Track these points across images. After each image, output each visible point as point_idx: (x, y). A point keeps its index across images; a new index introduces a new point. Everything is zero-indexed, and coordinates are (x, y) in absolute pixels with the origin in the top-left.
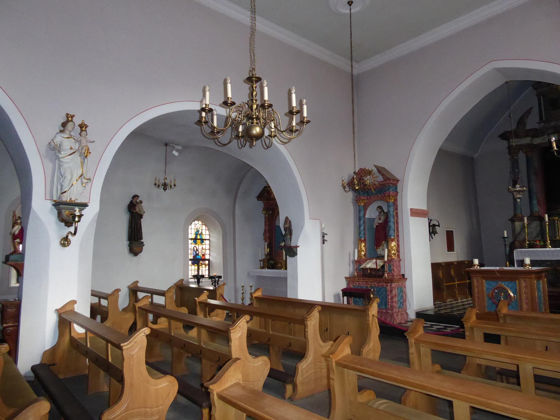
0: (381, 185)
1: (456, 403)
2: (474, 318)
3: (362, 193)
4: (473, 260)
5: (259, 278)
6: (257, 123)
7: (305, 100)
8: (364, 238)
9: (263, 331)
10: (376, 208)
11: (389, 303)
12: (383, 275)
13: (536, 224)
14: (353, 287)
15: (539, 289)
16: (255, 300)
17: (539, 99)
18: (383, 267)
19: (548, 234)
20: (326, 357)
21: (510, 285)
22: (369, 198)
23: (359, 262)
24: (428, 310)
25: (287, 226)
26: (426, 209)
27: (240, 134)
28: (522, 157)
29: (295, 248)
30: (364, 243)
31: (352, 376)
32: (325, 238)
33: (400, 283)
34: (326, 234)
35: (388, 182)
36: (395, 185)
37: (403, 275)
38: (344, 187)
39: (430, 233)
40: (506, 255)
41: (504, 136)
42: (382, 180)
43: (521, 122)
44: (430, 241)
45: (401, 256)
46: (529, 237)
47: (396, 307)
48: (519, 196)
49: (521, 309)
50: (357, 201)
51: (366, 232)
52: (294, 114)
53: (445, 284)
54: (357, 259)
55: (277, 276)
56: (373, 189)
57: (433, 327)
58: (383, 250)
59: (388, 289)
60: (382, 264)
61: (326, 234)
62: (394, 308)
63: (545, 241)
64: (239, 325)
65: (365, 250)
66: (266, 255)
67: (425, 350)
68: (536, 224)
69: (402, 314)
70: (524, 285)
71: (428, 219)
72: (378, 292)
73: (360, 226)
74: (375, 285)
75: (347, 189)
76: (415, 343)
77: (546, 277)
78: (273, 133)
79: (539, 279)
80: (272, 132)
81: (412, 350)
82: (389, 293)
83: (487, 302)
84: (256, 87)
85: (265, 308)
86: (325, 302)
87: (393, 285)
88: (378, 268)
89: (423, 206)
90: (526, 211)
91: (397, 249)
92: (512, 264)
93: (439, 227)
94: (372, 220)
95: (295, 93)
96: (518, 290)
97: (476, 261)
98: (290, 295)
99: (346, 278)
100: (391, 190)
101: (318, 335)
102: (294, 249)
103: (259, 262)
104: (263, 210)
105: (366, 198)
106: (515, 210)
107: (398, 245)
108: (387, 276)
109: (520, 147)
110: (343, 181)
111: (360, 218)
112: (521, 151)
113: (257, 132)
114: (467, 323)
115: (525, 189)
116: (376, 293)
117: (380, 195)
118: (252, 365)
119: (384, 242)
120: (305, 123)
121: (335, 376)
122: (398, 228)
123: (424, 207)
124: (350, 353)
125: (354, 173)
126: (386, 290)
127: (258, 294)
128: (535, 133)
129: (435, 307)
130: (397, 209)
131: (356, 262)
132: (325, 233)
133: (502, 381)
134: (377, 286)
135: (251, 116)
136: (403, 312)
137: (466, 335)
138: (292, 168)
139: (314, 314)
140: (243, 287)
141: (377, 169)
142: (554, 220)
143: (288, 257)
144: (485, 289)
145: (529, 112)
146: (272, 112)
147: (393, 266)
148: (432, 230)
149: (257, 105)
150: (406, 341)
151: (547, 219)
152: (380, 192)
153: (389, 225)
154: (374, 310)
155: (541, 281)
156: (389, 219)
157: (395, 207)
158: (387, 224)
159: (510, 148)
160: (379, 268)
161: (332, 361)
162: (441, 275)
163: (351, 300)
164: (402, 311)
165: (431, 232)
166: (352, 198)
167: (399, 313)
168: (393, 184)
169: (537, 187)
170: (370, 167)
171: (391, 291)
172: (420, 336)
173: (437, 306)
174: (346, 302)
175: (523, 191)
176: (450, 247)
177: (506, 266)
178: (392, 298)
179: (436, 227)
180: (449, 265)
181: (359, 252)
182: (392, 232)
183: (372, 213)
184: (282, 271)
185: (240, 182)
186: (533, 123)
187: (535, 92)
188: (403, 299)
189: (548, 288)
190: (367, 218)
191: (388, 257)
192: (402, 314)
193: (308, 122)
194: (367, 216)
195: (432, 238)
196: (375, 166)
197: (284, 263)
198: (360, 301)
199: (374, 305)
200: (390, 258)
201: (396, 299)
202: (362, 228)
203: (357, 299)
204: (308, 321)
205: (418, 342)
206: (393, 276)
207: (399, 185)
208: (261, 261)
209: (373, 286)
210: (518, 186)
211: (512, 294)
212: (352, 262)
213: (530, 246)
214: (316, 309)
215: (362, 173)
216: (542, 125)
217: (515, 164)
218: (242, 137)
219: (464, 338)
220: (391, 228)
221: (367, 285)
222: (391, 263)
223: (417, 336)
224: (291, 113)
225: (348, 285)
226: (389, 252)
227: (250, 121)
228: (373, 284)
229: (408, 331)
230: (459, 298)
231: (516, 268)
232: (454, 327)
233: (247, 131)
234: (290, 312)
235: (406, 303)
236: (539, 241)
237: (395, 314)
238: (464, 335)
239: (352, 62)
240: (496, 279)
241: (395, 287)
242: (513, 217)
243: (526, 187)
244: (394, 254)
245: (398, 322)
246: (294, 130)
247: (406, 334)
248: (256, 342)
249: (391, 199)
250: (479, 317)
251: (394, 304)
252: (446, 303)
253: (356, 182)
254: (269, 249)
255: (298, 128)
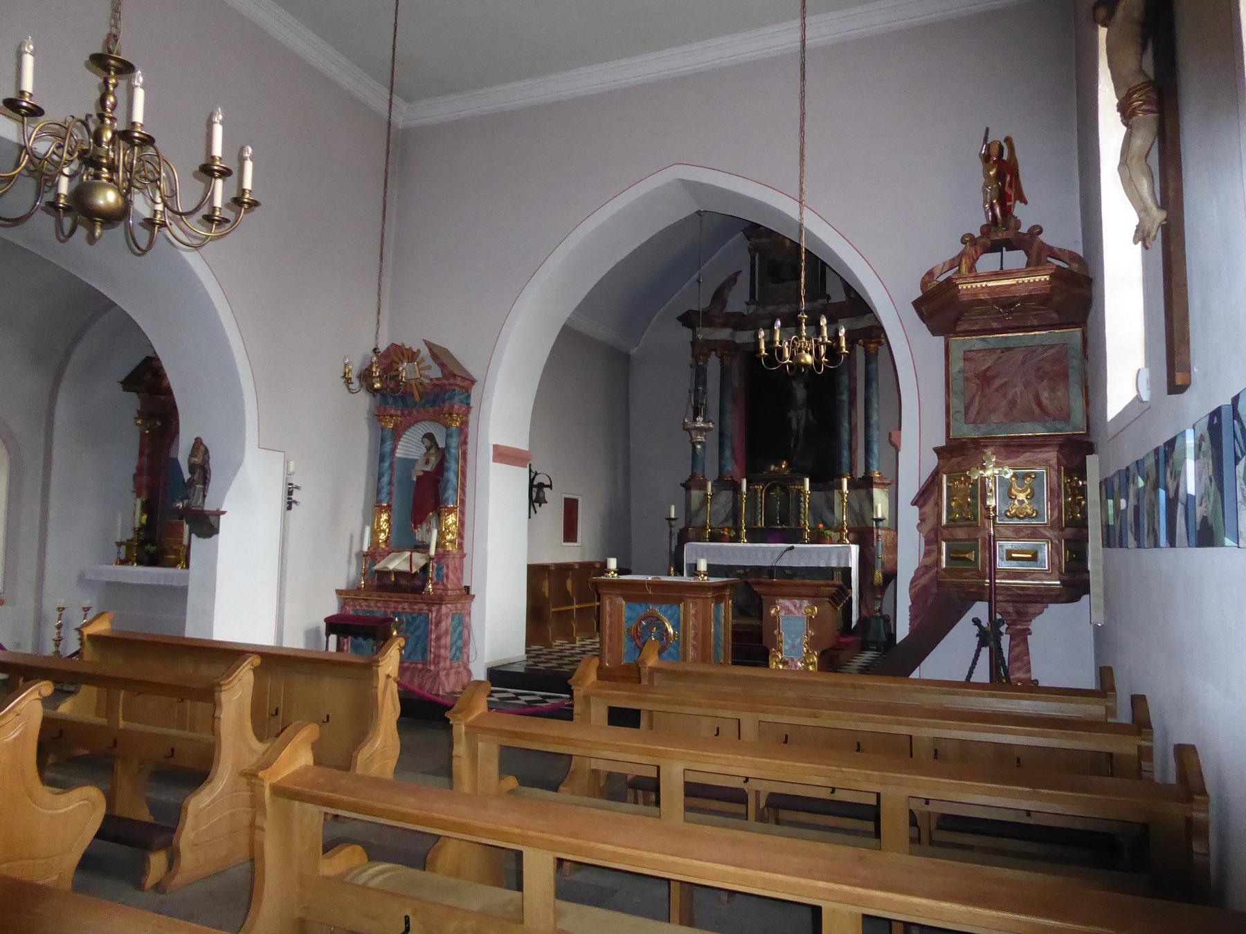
0: (435, 386)
1: (530, 855)
2: (593, 677)
3: (390, 400)
4: (606, 560)
5: (114, 587)
6: (110, 180)
7: (250, 150)
8: (389, 502)
9: (103, 721)
10: (421, 437)
11: (432, 650)
12: (424, 586)
13: (726, 496)
14: (354, 614)
15: (717, 620)
16: (87, 644)
17: (753, 258)
18: (425, 569)
19: (743, 516)
20: (251, 776)
21: (669, 612)
22: (406, 412)
23: (372, 556)
24: (513, 663)
25: (196, 460)
26: (527, 449)
27: (62, 201)
28: (713, 365)
29: (216, 515)
30: (387, 514)
31: (310, 818)
32: (294, 497)
33: (459, 606)
34: (297, 488)
35: (452, 381)
36: (467, 391)
37: (467, 589)
38: (348, 381)
39: (532, 502)
40: (670, 553)
41: (688, 319)
42: (440, 375)
43: (719, 296)
44: (530, 517)
45: (466, 549)
46: (712, 521)
47: (445, 658)
48: (700, 438)
49: (684, 659)
50: (379, 416)
51: (395, 489)
52: (213, 176)
53: (553, 610)
54: (369, 548)
55: (155, 583)
56: (416, 394)
57: (520, 699)
58: (429, 531)
59: (432, 618)
60: (422, 562)
61: (297, 488)
62: (441, 660)
63: (738, 530)
64: (17, 709)
65: (387, 530)
66: (137, 531)
67: (488, 749)
68: (726, 496)
69: (457, 673)
70: (692, 612)
71: (530, 471)
72: (409, 623)
73: (380, 476)
74: (403, 609)
75: (356, 384)
76: (466, 732)
77: (731, 597)
78: (159, 216)
79: (719, 599)
80: (155, 211)
81: (460, 749)
82: (433, 627)
83: (626, 645)
84: (115, 86)
85: (117, 665)
86: (282, 648)
87: (444, 610)
88: (413, 572)
89: (521, 442)
90: (711, 472)
91: (459, 530)
92: (679, 571)
93: (551, 489)
94: (409, 463)
95: (222, 123)
96: (682, 622)
97: (613, 563)
98: (192, 631)
99: (339, 592)
100: (457, 399)
101: (249, 724)
102: (212, 519)
103: (115, 548)
104: (137, 416)
105: (399, 413)
106: (694, 466)
107: (462, 523)
108: (433, 589)
109: (711, 345)
110: (346, 365)
111: (382, 456)
112: (714, 353)
113: (108, 204)
114: (579, 688)
115: (711, 426)
116: (404, 626)
117: (431, 410)
118: (50, 812)
119: (431, 514)
120: (246, 206)
121: (269, 823)
122: (465, 486)
123: (522, 444)
124: (311, 762)
125: (375, 350)
126: (427, 621)
127: (101, 627)
128: (740, 322)
129: (528, 657)
130: (465, 443)
131: (366, 555)
132: (295, 484)
133: (636, 802)
134: (409, 610)
135: (94, 159)
136: (461, 669)
137: (574, 712)
138: (223, 323)
139: (241, 674)
140: (61, 609)
141: (430, 350)
142: (756, 490)
143: (193, 536)
144: (624, 620)
145: (732, 280)
146: (156, 158)
147: (448, 567)
148: (536, 494)
149: (114, 133)
150: (448, 728)
151: (744, 489)
152: (433, 403)
153: (444, 478)
154: (390, 662)
155: (723, 604)
156: (446, 465)
157: (463, 437)
158: (442, 475)
159: (694, 342)
160: (416, 572)
161: (263, 786)
162: (546, 589)
163: (348, 641)
164: (459, 667)
165: (534, 499)
166: (368, 408)
167: (452, 671)
168: (462, 387)
169: (735, 424)
170: (414, 342)
171: (438, 624)
172: (478, 718)
173: (533, 654)
174: (333, 647)
175: (709, 429)
176: (570, 533)
177: (669, 575)
178: (438, 638)
179: (545, 490)
180: (563, 570)
181: (375, 533)
182: (450, 493)
183: (410, 447)
184: (178, 570)
185: (76, 339)
186: (737, 301)
187: (747, 243)
188: (462, 639)
189: (733, 617)
190: (400, 458)
191: (437, 547)
192: (457, 673)
193: (254, 204)
194: (399, 453)
195: (536, 512)
196: (426, 343)
197: (182, 555)
198: (367, 644)
199: (393, 652)
200: (441, 550)
201: (446, 641)
202: (385, 479)
203: (360, 640)
204: (223, 693)
205: (472, 729)
206: (446, 589)
207: (474, 392)
208: (119, 544)
209: (400, 610)
210: (700, 419)
211: (671, 630)
212: (357, 555)
213: (714, 538)
214: (245, 663)
215: (393, 356)
216: (752, 308)
217: (700, 376)
218: (67, 209)
219: (571, 719)
220: (450, 483)
221: (385, 608)
222: (443, 561)
223: (471, 718)
224: (207, 171)
225: (342, 607)
226: (441, 535)
227: (91, 170)
228: (400, 606)
229: (452, 710)
230: (577, 638)
231: (685, 578)
232: (561, 697)
233: (81, 197)
234: (186, 670)
235: (469, 649)
236: (729, 528)
237: (442, 674)
238: (571, 712)
239: (391, 94)
240: (646, 599)
241: (447, 613)
242: (689, 480)
243: (713, 423)
244: (451, 541)
245: (448, 689)
246: (216, 218)
247: (447, 715)
248: (83, 752)
249: (454, 420)
250: (603, 674)
251: (442, 651)
252: (551, 648)
253: (376, 373)
254: (145, 517)
255: (230, 215)
